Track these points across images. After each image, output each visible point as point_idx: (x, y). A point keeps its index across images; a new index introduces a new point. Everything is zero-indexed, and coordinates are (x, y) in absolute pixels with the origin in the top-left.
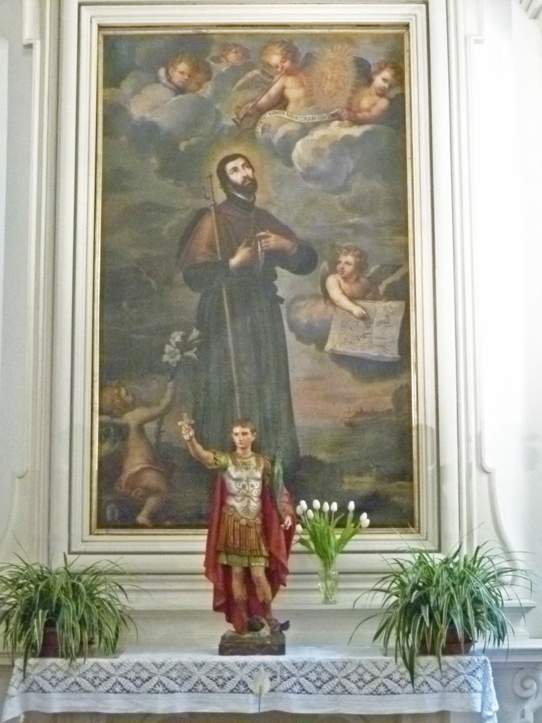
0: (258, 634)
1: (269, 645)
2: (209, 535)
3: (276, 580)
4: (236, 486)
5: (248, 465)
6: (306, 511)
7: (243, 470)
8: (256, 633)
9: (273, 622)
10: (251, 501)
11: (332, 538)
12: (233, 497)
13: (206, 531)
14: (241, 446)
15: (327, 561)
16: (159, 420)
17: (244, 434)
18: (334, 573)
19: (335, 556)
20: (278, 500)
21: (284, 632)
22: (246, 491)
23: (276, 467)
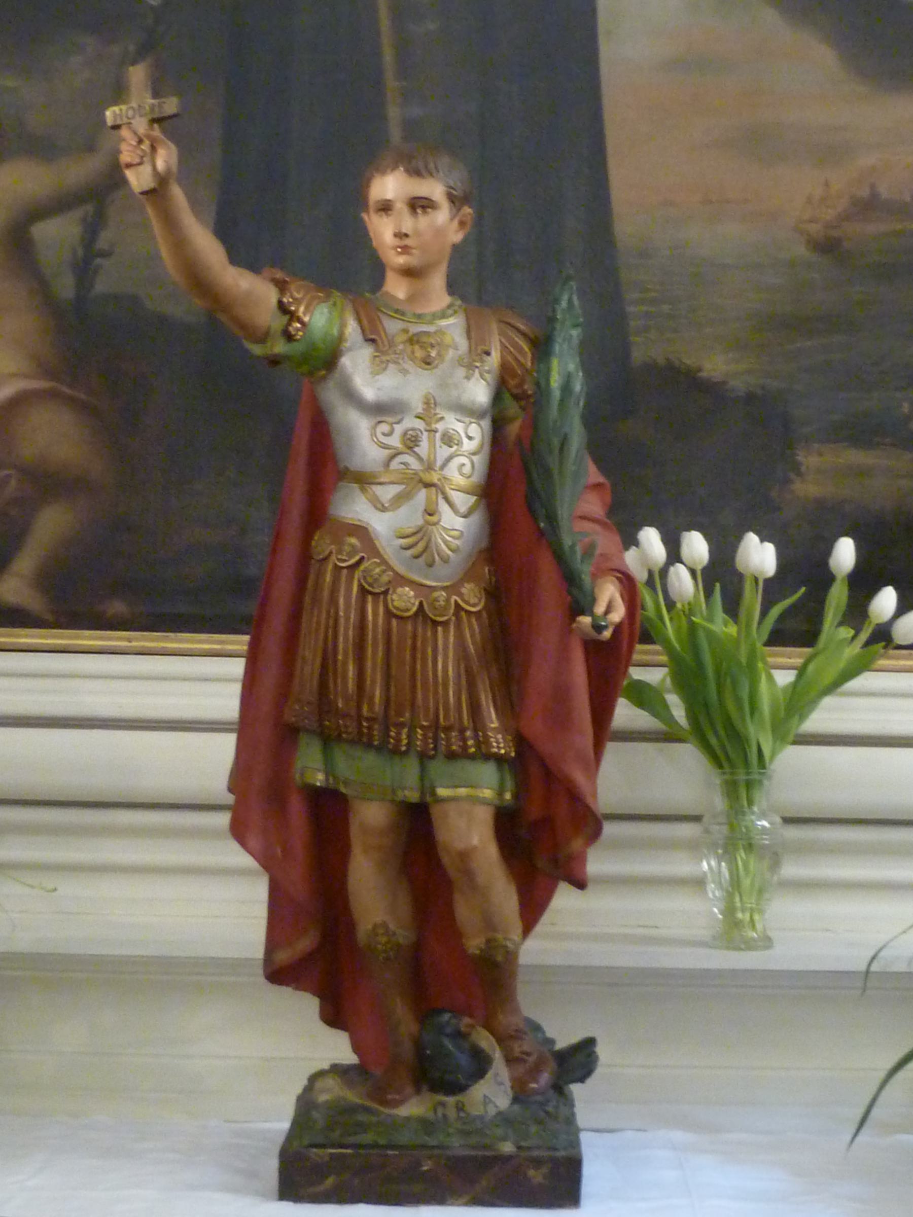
0: (460, 1108)
1: (508, 1158)
2: (254, 646)
3: (541, 863)
4: (373, 434)
5: (432, 346)
6: (664, 572)
7: (409, 365)
8: (451, 1100)
9: (526, 1045)
10: (444, 507)
11: (763, 686)
12: (363, 490)
13: (240, 643)
14: (401, 260)
15: (742, 777)
16: (89, 208)
17: (419, 205)
18: (765, 823)
19: (773, 755)
20: (563, 513)
21: (576, 1089)
22: (420, 459)
23: (555, 363)
